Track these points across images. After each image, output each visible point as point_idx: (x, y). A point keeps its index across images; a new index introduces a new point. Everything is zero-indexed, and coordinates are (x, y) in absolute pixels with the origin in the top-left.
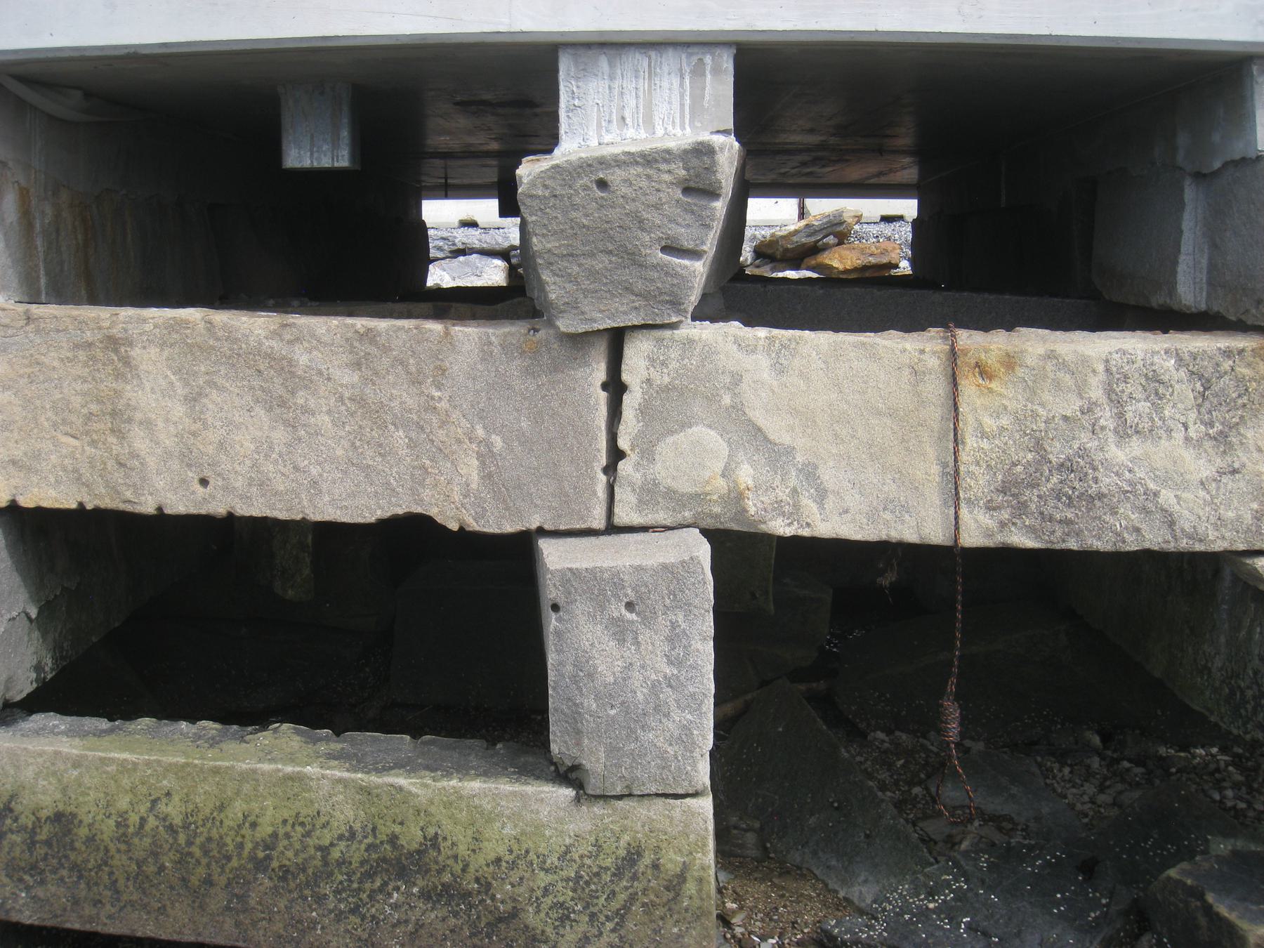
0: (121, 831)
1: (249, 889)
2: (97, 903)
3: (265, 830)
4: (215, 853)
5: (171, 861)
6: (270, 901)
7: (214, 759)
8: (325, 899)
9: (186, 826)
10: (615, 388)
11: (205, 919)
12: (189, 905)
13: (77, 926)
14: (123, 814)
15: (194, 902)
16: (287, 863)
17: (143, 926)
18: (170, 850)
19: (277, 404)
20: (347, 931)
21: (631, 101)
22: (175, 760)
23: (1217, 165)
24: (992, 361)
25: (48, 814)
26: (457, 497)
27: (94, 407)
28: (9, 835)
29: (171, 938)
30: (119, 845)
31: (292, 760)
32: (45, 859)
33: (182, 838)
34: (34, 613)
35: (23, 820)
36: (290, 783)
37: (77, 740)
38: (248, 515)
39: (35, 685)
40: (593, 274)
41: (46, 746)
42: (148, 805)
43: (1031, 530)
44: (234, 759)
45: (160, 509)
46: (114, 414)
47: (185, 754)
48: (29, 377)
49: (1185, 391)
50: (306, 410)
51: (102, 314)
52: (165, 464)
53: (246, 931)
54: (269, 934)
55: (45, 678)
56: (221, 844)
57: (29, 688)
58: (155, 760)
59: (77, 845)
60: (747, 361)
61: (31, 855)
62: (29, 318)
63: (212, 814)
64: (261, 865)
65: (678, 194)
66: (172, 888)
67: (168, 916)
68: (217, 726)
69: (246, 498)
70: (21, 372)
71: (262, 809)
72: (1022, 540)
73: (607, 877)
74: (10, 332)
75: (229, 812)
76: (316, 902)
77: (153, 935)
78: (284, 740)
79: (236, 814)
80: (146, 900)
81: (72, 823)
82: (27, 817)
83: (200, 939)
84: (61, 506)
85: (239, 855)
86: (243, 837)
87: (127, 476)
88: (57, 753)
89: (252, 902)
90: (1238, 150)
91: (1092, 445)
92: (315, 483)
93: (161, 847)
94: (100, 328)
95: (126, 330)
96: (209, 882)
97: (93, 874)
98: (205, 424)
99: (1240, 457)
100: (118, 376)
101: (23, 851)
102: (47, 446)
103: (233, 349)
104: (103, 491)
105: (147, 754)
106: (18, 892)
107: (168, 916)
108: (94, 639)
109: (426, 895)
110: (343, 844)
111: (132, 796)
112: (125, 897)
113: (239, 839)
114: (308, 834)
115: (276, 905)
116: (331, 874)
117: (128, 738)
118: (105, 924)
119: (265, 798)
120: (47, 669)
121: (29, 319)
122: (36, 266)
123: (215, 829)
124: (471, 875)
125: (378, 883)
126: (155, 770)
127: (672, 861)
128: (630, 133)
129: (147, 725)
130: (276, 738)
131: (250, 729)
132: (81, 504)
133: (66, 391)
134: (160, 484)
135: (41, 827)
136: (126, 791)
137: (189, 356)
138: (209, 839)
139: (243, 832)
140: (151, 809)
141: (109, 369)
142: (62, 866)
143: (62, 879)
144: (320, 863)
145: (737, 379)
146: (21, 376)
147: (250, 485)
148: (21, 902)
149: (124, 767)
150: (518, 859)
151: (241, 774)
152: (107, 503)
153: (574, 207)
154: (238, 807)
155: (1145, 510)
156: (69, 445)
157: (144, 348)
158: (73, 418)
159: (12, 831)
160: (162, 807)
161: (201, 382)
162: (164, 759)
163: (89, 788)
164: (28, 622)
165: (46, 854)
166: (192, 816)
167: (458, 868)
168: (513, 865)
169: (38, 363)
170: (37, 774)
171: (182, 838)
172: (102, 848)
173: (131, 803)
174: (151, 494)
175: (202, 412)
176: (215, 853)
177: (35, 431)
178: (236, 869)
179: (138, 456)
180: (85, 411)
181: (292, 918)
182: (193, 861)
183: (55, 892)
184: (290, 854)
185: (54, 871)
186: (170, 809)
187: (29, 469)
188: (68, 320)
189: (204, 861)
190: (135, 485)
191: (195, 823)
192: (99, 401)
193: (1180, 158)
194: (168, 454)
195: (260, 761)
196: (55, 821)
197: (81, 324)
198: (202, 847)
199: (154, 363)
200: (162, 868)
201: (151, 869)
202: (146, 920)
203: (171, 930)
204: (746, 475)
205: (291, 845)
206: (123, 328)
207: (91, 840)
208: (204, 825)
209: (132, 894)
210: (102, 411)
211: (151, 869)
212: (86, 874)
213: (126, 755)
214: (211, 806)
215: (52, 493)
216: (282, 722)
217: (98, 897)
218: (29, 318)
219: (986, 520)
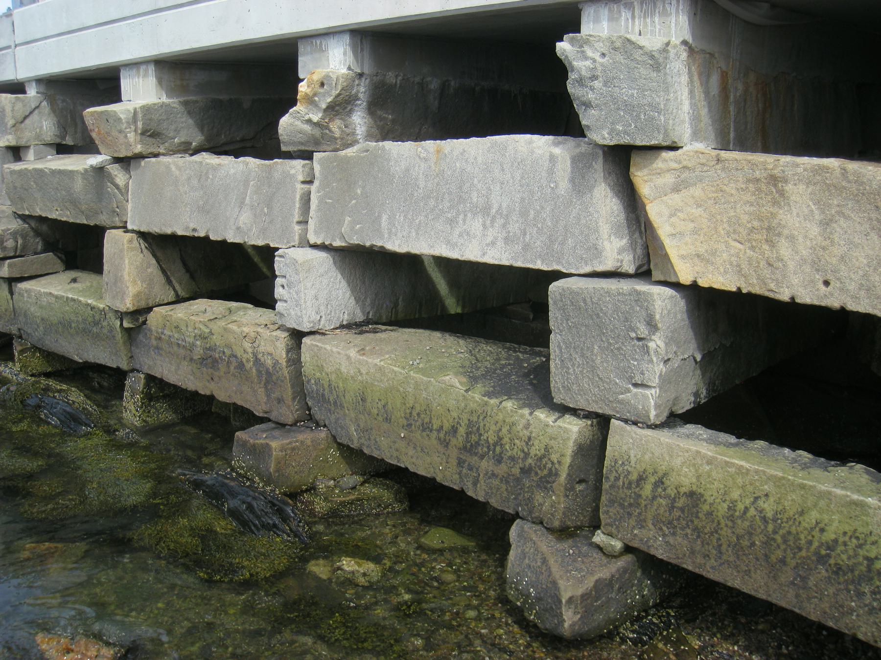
0: (730, 513)
1: (810, 574)
2: (707, 556)
3: (829, 536)
4: (791, 543)
5: (760, 541)
6: (823, 586)
7: (804, 479)
8: (863, 595)
9: (775, 520)
11: (775, 586)
12: (766, 573)
13: (690, 568)
14: (734, 502)
15: (770, 572)
16: (841, 563)
17: (733, 579)
18: (760, 533)
20: (875, 623)
22: (776, 473)
25: (686, 491)
27: (756, 224)
28: (659, 499)
29: (749, 593)
30: (727, 522)
31: (859, 491)
32: (678, 519)
33: (770, 527)
34: (699, 358)
35: (669, 491)
36: (854, 507)
37: (713, 446)
38: (855, 310)
39: (692, 405)
41: (693, 446)
42: (752, 499)
44: (817, 481)
45: (793, 298)
46: (769, 229)
47: (783, 470)
48: (715, 199)
51: (769, 159)
52: (800, 268)
53: (802, 602)
54: (817, 609)
55: (700, 402)
57: (688, 407)
58: (761, 471)
59: (700, 515)
61: (670, 514)
62: (718, 160)
63: (794, 515)
64: (822, 559)
67: (751, 577)
68: (810, 456)
69: (855, 298)
70: (710, 196)
71: (830, 521)
74: (705, 169)
75: (806, 517)
76: (857, 596)
77: (738, 587)
78: (855, 476)
79: (811, 520)
80: (738, 563)
81: (700, 500)
82: (672, 489)
83: (769, 599)
84: (726, 289)
85: (808, 549)
86: (813, 537)
87: (773, 273)
88: (698, 452)
89: (811, 583)
93: (755, 530)
94: (765, 169)
95: (783, 172)
96: (783, 561)
97: (707, 536)
98: (832, 242)
100: (775, 203)
101: (666, 511)
102: (722, 247)
103: (860, 190)
104: (755, 281)
105: (758, 465)
106: (657, 536)
107: (751, 577)
108: (737, 382)
111: (741, 491)
112: (724, 557)
113: (810, 538)
114: (860, 546)
115: (827, 590)
116: (871, 579)
117: (746, 452)
118: (709, 572)
119: (834, 513)
120: (702, 396)
121: (718, 160)
122: (729, 124)
123: (794, 527)
126: (761, 477)
129: (761, 445)
130: (850, 473)
131: (833, 463)
132: (739, 289)
133: (738, 211)
134: (795, 280)
135: (679, 498)
136: (739, 487)
137: (826, 192)
138: (789, 533)
139: (814, 533)
140: (753, 503)
141: (769, 198)
142: (688, 526)
143: (686, 535)
144: (865, 569)
146: (710, 199)
147: (860, 289)
148: (658, 543)
149: (740, 469)
151: (820, 492)
152: (757, 290)
154: (814, 515)
156: (736, 248)
157: (795, 185)
158: (741, 230)
159: (661, 497)
160: (760, 503)
161: (833, 212)
162: (768, 471)
163: (715, 480)
164: (694, 363)
165: (680, 516)
166: (780, 514)
169: (721, 191)
170: (683, 463)
171: (770, 527)
172: (716, 521)
173: (740, 495)
174: (788, 287)
175: (831, 233)
176: (791, 543)
177: (715, 236)
178: (804, 558)
179: (782, 260)
180: (749, 225)
181: (837, 602)
182: (775, 545)
184: (844, 557)
185: (683, 529)
186: (766, 506)
187: (708, 261)
188: (744, 163)
189: (783, 547)
190: (777, 280)
191: (781, 519)
192: (761, 220)
194: (804, 260)
195: (835, 486)
196: (689, 496)
197: (753, 165)
198: (783, 537)
199: (801, 195)
200: (753, 544)
201: (745, 543)
202: (736, 576)
203: (751, 587)
205: (846, 551)
206: (782, 170)
207: (710, 514)
208: (787, 522)
209: (729, 556)
210: (761, 226)
211: (745, 543)
212: (702, 535)
214: (795, 510)
215: (721, 279)
216: (858, 462)
217: (707, 553)
218: (718, 160)
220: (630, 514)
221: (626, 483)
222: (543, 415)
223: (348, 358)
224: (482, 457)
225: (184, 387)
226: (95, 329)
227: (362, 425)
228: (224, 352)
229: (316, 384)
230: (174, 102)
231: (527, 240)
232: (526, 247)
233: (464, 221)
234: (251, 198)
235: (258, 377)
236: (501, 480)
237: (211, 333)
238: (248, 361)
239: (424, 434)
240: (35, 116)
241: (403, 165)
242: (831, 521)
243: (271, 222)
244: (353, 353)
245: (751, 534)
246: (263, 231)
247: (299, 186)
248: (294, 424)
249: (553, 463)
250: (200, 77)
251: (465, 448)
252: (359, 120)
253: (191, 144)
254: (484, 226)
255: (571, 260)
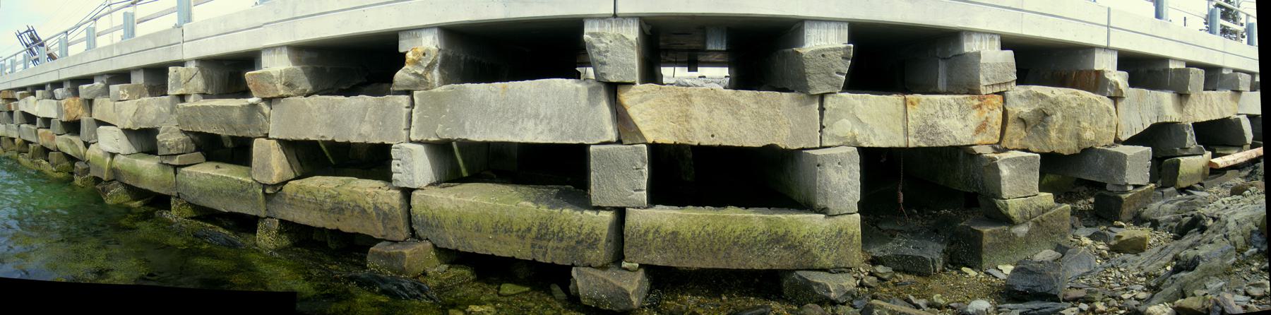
9: (713, 234)
10: (822, 110)
14: (694, 231)
19: (733, 113)
21: (822, 35)
23: (950, 56)
24: (914, 101)
26: (784, 139)
27: (680, 114)
33: (712, 237)
35: (661, 234)
40: (819, 79)
43: (925, 142)
49: (956, 107)
50: (743, 115)
56: (724, 238)
60: (856, 102)
64: (735, 243)
65: (841, 58)
66: (707, 252)
69: (726, 140)
72: (923, 145)
73: (833, 238)
89: (732, 255)
90: (957, 52)
91: (938, 121)
92: (745, 136)
99: (968, 123)
100: (688, 105)
102: (665, 125)
109: (785, 248)
110: (761, 236)
121: (660, 88)
124: (796, 241)
125: (771, 245)
127: (850, 231)
128: (822, 43)
132: (675, 142)
134: (700, 136)
143: (672, 251)
145: (853, 106)
149: (695, 217)
150: (811, 235)
152: (684, 142)
153: (816, 61)
155: (950, 136)
160: (706, 228)
167: (793, 239)
168: (808, 237)
171: (712, 237)
183: (670, 255)
192: (682, 112)
193: (938, 54)
194: (702, 127)
200: (705, 246)
204: (856, 131)
213: (695, 214)
219: (915, 140)
220: (641, 250)
221: (638, 235)
222: (587, 212)
223: (450, 200)
224: (549, 240)
225: (313, 226)
226: (241, 194)
227: (458, 236)
228: (349, 204)
229: (421, 217)
230: (298, 68)
231: (563, 129)
232: (563, 133)
233: (522, 122)
234: (369, 117)
235: (377, 217)
236: (563, 250)
237: (339, 194)
238: (369, 208)
239: (507, 234)
240: (194, 79)
241: (479, 95)
242: (738, 227)
243: (385, 130)
244: (452, 197)
245: (703, 243)
246: (380, 135)
247: (405, 109)
248: (405, 240)
249: (597, 235)
250: (306, 55)
251: (537, 238)
252: (436, 75)
253: (306, 90)
254: (536, 124)
255: (590, 137)
